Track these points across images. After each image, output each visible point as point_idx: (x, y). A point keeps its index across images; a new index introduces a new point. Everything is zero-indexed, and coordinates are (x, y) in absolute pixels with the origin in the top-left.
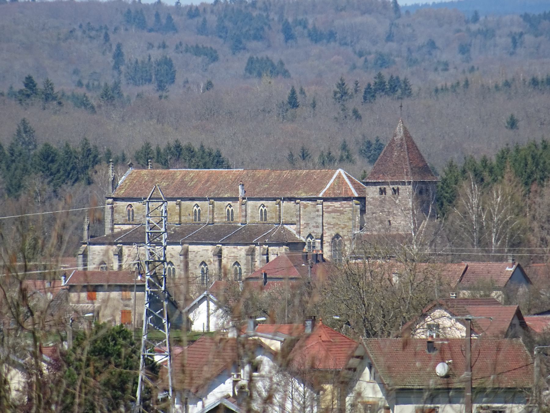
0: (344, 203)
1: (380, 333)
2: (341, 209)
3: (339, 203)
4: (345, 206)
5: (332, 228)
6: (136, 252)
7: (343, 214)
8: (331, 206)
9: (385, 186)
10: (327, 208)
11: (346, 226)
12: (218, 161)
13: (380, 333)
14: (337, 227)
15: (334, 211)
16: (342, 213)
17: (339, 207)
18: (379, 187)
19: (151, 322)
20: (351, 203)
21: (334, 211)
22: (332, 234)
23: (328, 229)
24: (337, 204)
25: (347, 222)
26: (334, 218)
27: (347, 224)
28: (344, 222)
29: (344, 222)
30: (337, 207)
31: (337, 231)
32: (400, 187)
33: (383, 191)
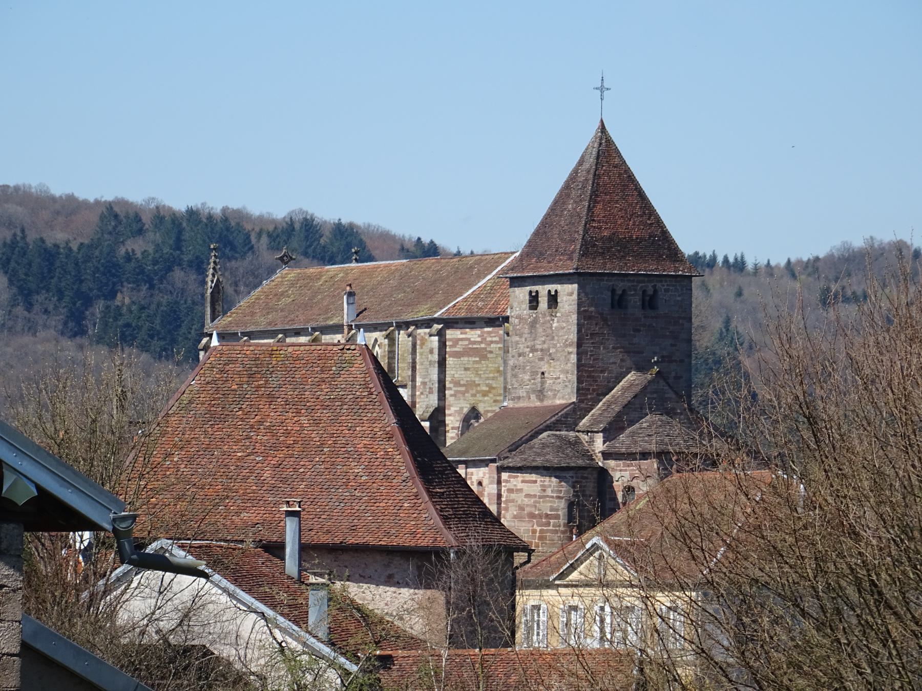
0: (489, 333)
2: (483, 346)
3: (478, 332)
4: (489, 339)
5: (463, 393)
7: (484, 357)
8: (462, 339)
11: (491, 388)
14: (474, 392)
15: (466, 352)
18: (528, 288)
21: (466, 352)
22: (462, 408)
24: (474, 335)
25: (493, 378)
26: (466, 369)
28: (488, 378)
29: (488, 378)
30: (475, 343)
31: (472, 401)
32: (558, 287)
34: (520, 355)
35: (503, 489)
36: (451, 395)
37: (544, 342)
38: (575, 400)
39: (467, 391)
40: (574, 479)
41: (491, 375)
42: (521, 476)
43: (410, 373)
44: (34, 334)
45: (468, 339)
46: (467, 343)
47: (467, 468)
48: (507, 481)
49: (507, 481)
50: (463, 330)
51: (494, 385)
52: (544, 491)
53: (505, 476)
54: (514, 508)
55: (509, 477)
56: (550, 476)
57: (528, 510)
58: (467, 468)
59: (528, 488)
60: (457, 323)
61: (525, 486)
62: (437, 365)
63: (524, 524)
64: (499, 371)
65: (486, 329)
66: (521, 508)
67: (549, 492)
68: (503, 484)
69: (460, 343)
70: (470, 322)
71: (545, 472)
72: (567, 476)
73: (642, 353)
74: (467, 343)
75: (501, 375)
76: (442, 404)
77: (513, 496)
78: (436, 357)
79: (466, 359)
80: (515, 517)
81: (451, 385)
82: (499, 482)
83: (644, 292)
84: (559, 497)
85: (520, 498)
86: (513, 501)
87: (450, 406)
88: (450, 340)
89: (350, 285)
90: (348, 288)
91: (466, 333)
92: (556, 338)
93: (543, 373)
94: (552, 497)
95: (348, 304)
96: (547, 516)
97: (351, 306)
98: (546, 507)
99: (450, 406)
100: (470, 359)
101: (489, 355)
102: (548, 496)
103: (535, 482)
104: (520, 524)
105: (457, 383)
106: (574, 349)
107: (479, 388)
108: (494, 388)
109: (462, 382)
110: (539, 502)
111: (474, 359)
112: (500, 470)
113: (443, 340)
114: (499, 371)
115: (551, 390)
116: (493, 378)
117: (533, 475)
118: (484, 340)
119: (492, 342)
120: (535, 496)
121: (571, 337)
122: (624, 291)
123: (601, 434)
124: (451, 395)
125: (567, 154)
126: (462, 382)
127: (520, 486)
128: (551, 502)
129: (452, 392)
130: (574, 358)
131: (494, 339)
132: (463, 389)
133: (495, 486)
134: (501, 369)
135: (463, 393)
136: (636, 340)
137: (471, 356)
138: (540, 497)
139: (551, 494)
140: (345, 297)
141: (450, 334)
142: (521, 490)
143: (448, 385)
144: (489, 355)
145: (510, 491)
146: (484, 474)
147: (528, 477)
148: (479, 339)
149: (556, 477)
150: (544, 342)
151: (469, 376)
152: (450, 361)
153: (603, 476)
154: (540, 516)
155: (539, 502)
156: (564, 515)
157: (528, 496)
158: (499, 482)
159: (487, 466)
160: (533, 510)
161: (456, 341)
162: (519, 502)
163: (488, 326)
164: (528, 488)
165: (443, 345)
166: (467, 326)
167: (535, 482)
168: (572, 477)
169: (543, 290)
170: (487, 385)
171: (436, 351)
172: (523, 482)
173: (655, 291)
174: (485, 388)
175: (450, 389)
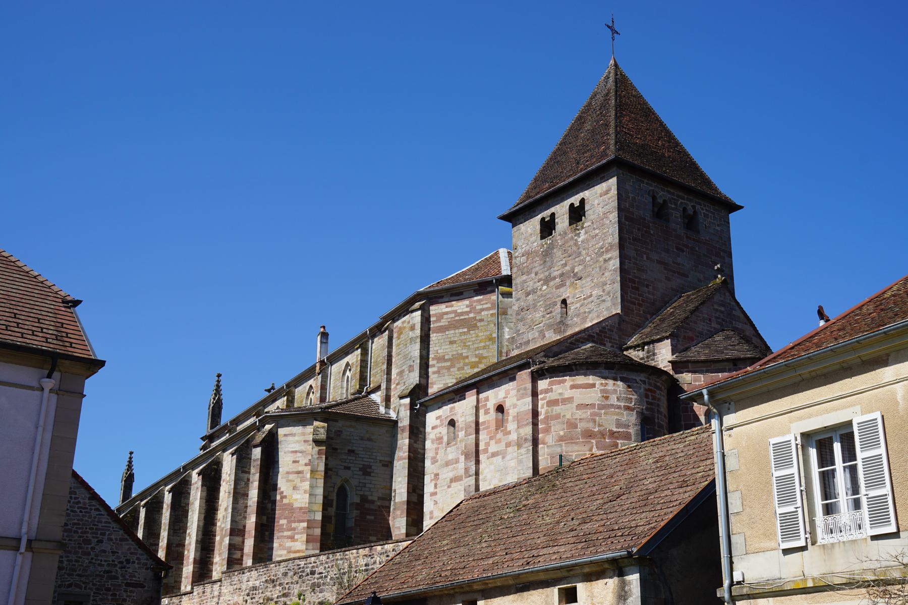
1: (519, 317)
2: (472, 315)
3: (467, 302)
4: (479, 307)
5: (448, 368)
6: (493, 442)
7: (475, 327)
8: (447, 313)
9: (552, 210)
10: (438, 320)
12: (875, 538)
13: (519, 317)
16: (471, 325)
17: (467, 313)
18: (539, 217)
19: (386, 535)
20: (494, 297)
23: (438, 372)
24: (461, 306)
25: (484, 348)
26: (451, 343)
27: (484, 353)
30: (462, 314)
33: (548, 228)
34: (528, 294)
35: (540, 403)
36: (434, 373)
37: (565, 265)
38: (619, 311)
39: (452, 366)
40: (647, 387)
41: (482, 344)
42: (569, 380)
43: (385, 366)
44: (172, 567)
45: (455, 312)
46: (453, 315)
47: (478, 393)
48: (546, 391)
49: (546, 391)
50: (449, 304)
51: (486, 355)
52: (607, 398)
53: (542, 384)
54: (558, 427)
55: (551, 384)
56: (615, 379)
57: (581, 426)
58: (478, 393)
59: (580, 396)
60: (461, 293)
61: (577, 394)
62: (419, 340)
63: (576, 448)
64: (491, 339)
65: (475, 298)
66: (572, 425)
67: (613, 400)
68: (540, 397)
69: (445, 317)
70: (454, 292)
71: (606, 373)
72: (638, 379)
73: (687, 277)
74: (453, 315)
75: (493, 342)
76: (424, 381)
77: (557, 409)
78: (418, 332)
79: (453, 332)
80: (561, 439)
81: (435, 362)
82: (535, 394)
83: (685, 209)
84: (628, 408)
85: (568, 412)
86: (558, 417)
87: (432, 383)
88: (435, 315)
89: (324, 327)
90: (322, 330)
91: (452, 306)
92: (584, 252)
93: (564, 302)
94: (619, 407)
95: (321, 342)
96: (612, 434)
97: (324, 345)
98: (609, 422)
99: (432, 383)
100: (457, 331)
101: (479, 324)
102: (612, 406)
103: (593, 386)
104: (570, 448)
105: (441, 359)
106: (616, 253)
107: (467, 361)
108: (485, 358)
109: (446, 357)
110: (600, 415)
111: (461, 331)
112: (537, 376)
113: (426, 315)
114: (491, 339)
115: (578, 315)
116: (484, 348)
117: (591, 377)
118: (472, 309)
119: (482, 310)
120: (592, 406)
121: (610, 240)
122: (665, 201)
123: (668, 342)
124: (434, 373)
125: (596, 78)
126: (446, 357)
127: (568, 393)
128: (617, 414)
129: (435, 369)
130: (615, 263)
131: (485, 306)
132: (448, 364)
133: (529, 399)
134: (495, 335)
135: (448, 368)
136: (679, 260)
137: (458, 328)
138: (601, 407)
139: (616, 403)
140: (319, 338)
141: (434, 310)
142: (570, 400)
143: (431, 362)
144: (479, 324)
145: (552, 403)
146: (507, 392)
147: (581, 380)
148: (468, 309)
149: (623, 380)
150: (565, 265)
151: (457, 349)
152: (433, 337)
153: (674, 387)
154: (602, 435)
155: (600, 415)
156: (637, 434)
157: (580, 406)
158: (535, 394)
159: (513, 379)
160: (590, 425)
161: (440, 316)
162: (568, 416)
163: (477, 295)
164: (580, 396)
165: (426, 321)
166: (452, 298)
167: (593, 386)
168: (644, 382)
169: (561, 210)
170: (476, 356)
171: (418, 326)
172: (573, 387)
173: (695, 212)
174: (474, 359)
175: (434, 366)
